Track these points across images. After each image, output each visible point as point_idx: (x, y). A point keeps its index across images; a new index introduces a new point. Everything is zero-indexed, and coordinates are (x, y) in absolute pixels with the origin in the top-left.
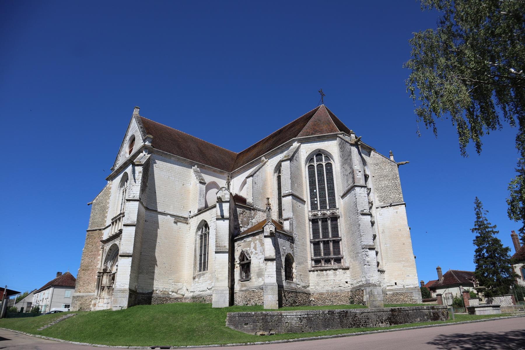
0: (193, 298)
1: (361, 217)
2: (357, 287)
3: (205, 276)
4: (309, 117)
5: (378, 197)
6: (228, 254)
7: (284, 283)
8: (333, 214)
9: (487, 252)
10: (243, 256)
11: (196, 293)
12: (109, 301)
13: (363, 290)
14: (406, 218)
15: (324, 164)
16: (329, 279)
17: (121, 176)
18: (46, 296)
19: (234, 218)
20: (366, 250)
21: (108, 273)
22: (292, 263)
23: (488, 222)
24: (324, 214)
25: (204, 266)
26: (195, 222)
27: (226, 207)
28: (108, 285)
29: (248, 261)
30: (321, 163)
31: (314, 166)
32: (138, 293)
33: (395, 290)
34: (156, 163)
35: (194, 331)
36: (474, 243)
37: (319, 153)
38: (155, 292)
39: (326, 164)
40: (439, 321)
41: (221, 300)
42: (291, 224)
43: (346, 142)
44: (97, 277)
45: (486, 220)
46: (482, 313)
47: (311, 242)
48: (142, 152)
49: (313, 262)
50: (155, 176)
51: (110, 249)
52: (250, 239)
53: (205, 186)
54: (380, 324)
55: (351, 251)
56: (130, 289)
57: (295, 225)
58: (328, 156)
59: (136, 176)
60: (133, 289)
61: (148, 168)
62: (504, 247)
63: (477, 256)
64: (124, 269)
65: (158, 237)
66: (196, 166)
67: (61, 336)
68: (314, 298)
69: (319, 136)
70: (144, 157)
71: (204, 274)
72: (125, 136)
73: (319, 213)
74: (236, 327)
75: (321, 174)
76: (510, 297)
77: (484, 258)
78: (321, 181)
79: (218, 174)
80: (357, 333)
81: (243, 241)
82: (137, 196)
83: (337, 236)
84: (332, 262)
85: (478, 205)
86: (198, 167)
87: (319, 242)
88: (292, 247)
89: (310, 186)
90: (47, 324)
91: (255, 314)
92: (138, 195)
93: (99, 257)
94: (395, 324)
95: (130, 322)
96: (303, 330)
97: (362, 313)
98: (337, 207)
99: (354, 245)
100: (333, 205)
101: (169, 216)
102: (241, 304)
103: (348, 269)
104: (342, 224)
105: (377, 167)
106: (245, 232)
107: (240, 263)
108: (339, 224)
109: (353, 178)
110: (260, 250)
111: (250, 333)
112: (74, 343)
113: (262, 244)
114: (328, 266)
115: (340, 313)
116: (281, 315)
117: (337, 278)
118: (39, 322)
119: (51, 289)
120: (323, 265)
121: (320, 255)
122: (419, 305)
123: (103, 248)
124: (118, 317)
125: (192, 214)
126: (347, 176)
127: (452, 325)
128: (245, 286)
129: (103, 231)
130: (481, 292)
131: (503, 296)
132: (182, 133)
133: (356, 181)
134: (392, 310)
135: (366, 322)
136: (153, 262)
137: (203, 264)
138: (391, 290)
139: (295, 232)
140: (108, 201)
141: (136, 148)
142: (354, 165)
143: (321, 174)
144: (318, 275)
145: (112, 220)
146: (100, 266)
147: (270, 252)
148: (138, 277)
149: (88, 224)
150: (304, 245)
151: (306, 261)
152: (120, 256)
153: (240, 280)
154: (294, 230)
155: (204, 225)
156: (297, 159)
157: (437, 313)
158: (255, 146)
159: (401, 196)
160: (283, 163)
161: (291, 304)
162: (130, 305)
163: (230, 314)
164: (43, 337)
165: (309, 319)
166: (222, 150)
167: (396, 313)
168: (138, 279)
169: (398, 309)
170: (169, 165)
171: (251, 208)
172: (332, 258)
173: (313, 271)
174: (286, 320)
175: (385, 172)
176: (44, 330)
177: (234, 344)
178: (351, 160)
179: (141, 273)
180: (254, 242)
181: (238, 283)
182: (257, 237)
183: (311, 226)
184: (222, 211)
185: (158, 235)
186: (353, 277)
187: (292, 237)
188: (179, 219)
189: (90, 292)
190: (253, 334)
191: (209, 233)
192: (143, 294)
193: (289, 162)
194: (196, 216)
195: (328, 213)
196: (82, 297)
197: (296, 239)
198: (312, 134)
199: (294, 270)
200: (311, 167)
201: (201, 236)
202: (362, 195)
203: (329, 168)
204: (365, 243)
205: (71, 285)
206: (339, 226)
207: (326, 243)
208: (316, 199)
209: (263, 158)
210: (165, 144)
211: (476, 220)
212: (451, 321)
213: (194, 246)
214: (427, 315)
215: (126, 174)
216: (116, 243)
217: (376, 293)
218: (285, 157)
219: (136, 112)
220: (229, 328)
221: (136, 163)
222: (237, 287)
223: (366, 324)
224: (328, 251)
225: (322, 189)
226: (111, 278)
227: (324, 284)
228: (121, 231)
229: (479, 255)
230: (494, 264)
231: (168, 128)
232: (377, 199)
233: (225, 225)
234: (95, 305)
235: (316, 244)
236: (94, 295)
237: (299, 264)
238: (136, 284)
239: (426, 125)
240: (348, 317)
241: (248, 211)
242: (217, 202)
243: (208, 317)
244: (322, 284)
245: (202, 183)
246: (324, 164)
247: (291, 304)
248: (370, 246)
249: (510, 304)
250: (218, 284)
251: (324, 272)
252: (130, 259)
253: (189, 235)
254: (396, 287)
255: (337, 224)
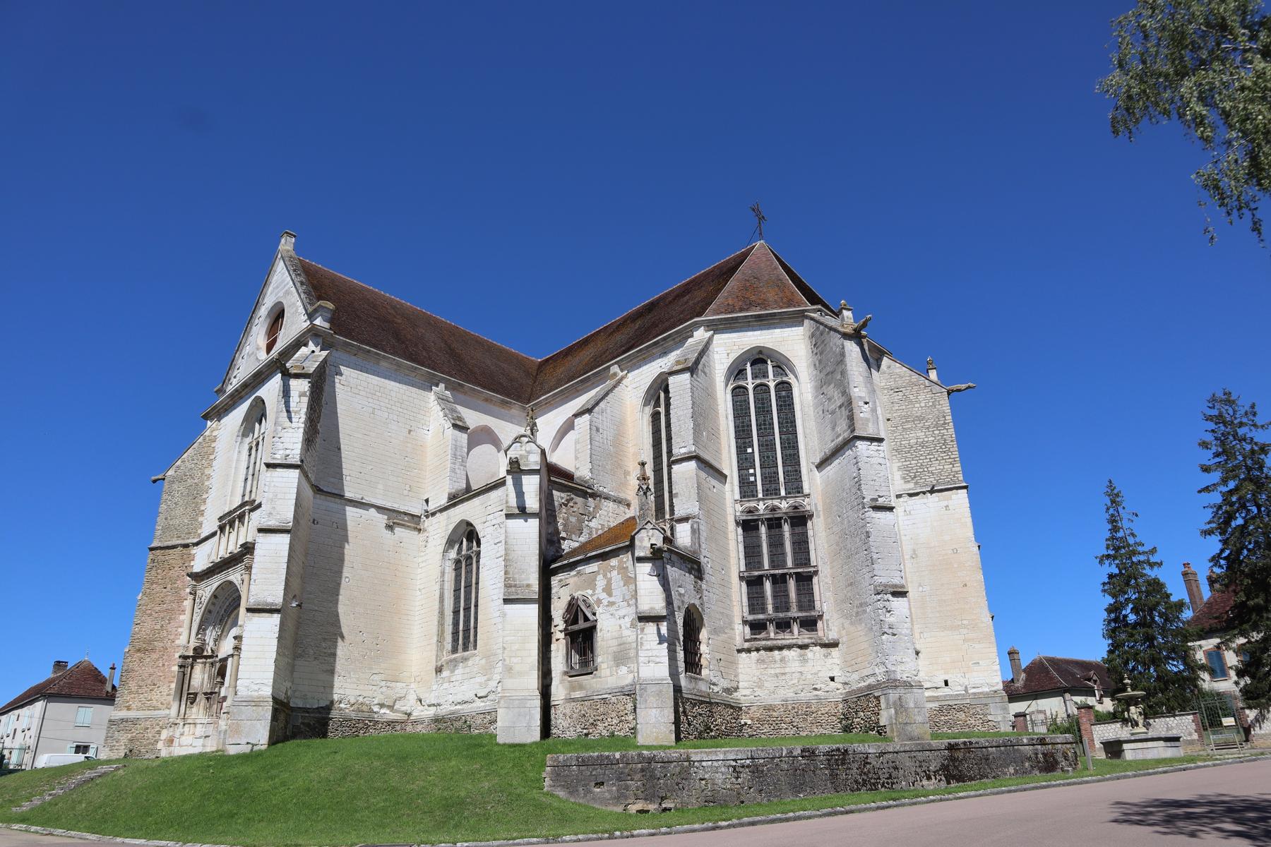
0: (437, 720)
1: (872, 514)
2: (860, 690)
3: (470, 663)
4: (728, 271)
5: (899, 469)
6: (536, 606)
7: (683, 682)
8: (796, 508)
9: (1135, 610)
10: (574, 613)
11: (445, 709)
12: (210, 730)
13: (877, 698)
14: (969, 520)
15: (772, 385)
16: (787, 670)
17: (244, 407)
18: (23, 724)
19: (548, 514)
20: (886, 597)
21: (206, 657)
22: (699, 631)
23: (1138, 540)
24: (774, 509)
25: (466, 638)
26: (439, 528)
27: (531, 484)
28: (207, 688)
29: (587, 625)
30: (764, 381)
31: (746, 389)
32: (292, 709)
33: (945, 698)
34: (341, 375)
35: (461, 803)
36: (1104, 591)
37: (759, 358)
38: (336, 705)
39: (776, 386)
40: (1058, 773)
41: (518, 726)
42: (695, 532)
43: (831, 329)
44: (176, 668)
45: (1133, 535)
46: (1140, 756)
47: (741, 578)
48: (306, 345)
49: (747, 629)
50: (339, 406)
51: (215, 596)
52: (593, 567)
53: (465, 436)
54: (925, 782)
55: (843, 601)
56: (274, 698)
57: (704, 534)
58: (782, 365)
59: (293, 405)
60: (282, 697)
61: (321, 383)
62: (1174, 599)
63: (1109, 622)
64: (258, 643)
65: (346, 563)
66: (442, 386)
67: (87, 824)
68: (752, 719)
69: (759, 316)
70: (311, 356)
71: (465, 659)
72: (257, 305)
73: (761, 506)
74: (571, 793)
75: (763, 409)
76: (1191, 717)
77: (1127, 625)
78: (765, 427)
79: (496, 409)
80: (879, 804)
81: (573, 573)
82: (295, 454)
83: (807, 562)
84: (795, 628)
85: (1114, 500)
86: (446, 388)
87: (761, 577)
88: (699, 590)
89: (737, 438)
90: (41, 794)
91: (623, 757)
92: (298, 451)
93: (182, 617)
94: (958, 781)
95: (283, 784)
96: (742, 798)
97: (882, 754)
98: (806, 491)
99: (851, 584)
100: (795, 485)
101: (372, 510)
102: (571, 734)
103: (834, 645)
104: (819, 535)
105: (897, 397)
106: (574, 552)
107: (565, 630)
108: (810, 533)
109: (851, 418)
110: (623, 599)
111: (610, 808)
112: (127, 840)
113: (630, 581)
114: (785, 638)
115: (829, 754)
116: (688, 759)
117: (808, 669)
118: (16, 790)
119: (39, 705)
120: (772, 635)
121: (764, 610)
122: (1006, 734)
123: (194, 593)
124: (247, 769)
125: (432, 507)
126: (833, 413)
127: (1094, 781)
128: (581, 687)
129: (194, 550)
130: (1136, 705)
131: (1174, 716)
132: (402, 305)
133: (857, 425)
134: (951, 747)
135: (890, 777)
136: (333, 632)
137: (463, 632)
138: (935, 699)
139: (704, 553)
140: (207, 472)
141: (285, 337)
142: (851, 386)
143: (763, 409)
144: (760, 661)
145: (221, 519)
146: (184, 638)
147: (652, 599)
148: (293, 666)
149: (154, 530)
150: (725, 584)
151: (730, 624)
152: (249, 610)
153: (566, 673)
154: (703, 546)
155: (468, 534)
156: (706, 370)
157: (1052, 755)
158: (585, 342)
159: (958, 467)
160: (671, 380)
161: (700, 733)
162: (275, 739)
163: (557, 760)
164: (33, 828)
165: (756, 770)
166: (502, 351)
167: (960, 755)
168: (292, 672)
169: (965, 743)
170: (375, 380)
171: (585, 491)
172: (795, 619)
173: (749, 651)
174: (701, 774)
175: (917, 410)
176: (32, 809)
177: (580, 837)
178: (843, 373)
179: (301, 656)
180: (605, 576)
181: (562, 681)
182: (614, 562)
183: (741, 538)
184: (520, 494)
185: (346, 558)
186: (849, 665)
187: (699, 564)
188: (398, 519)
189: (155, 708)
190: (619, 809)
191: (478, 554)
192: (306, 710)
193: (687, 375)
194: (441, 511)
195: (784, 505)
196: (135, 721)
197: (708, 567)
198: (741, 310)
199: (703, 648)
200: (739, 392)
201: (458, 562)
202: (873, 461)
203: (784, 393)
204: (884, 580)
205: (94, 694)
206: (811, 540)
207: (779, 581)
208: (751, 471)
209: (615, 369)
210: (365, 326)
211: (1108, 535)
212: (1086, 773)
213: (437, 587)
214: (1029, 759)
215: (260, 403)
216: (231, 578)
217: (912, 705)
218: (678, 363)
219: (286, 244)
220: (552, 795)
221: (293, 371)
222: (559, 691)
223: (891, 782)
224: (783, 601)
225: (767, 447)
226: (215, 670)
227: (777, 683)
228: (248, 549)
229: (1116, 620)
230: (1150, 639)
231: (369, 290)
232: (898, 475)
233: (528, 532)
234: (170, 741)
235: (753, 583)
236: (168, 717)
237: (715, 631)
238: (288, 684)
239: (1229, 214)
240: (847, 763)
241: (579, 500)
242: (508, 472)
243: (494, 768)
244: (769, 685)
245: (460, 427)
246: (772, 385)
247: (700, 733)
248: (896, 586)
249: (1190, 734)
250: (509, 683)
251: (776, 652)
252: (276, 619)
253: (426, 562)
254: (946, 691)
255: (805, 534)
